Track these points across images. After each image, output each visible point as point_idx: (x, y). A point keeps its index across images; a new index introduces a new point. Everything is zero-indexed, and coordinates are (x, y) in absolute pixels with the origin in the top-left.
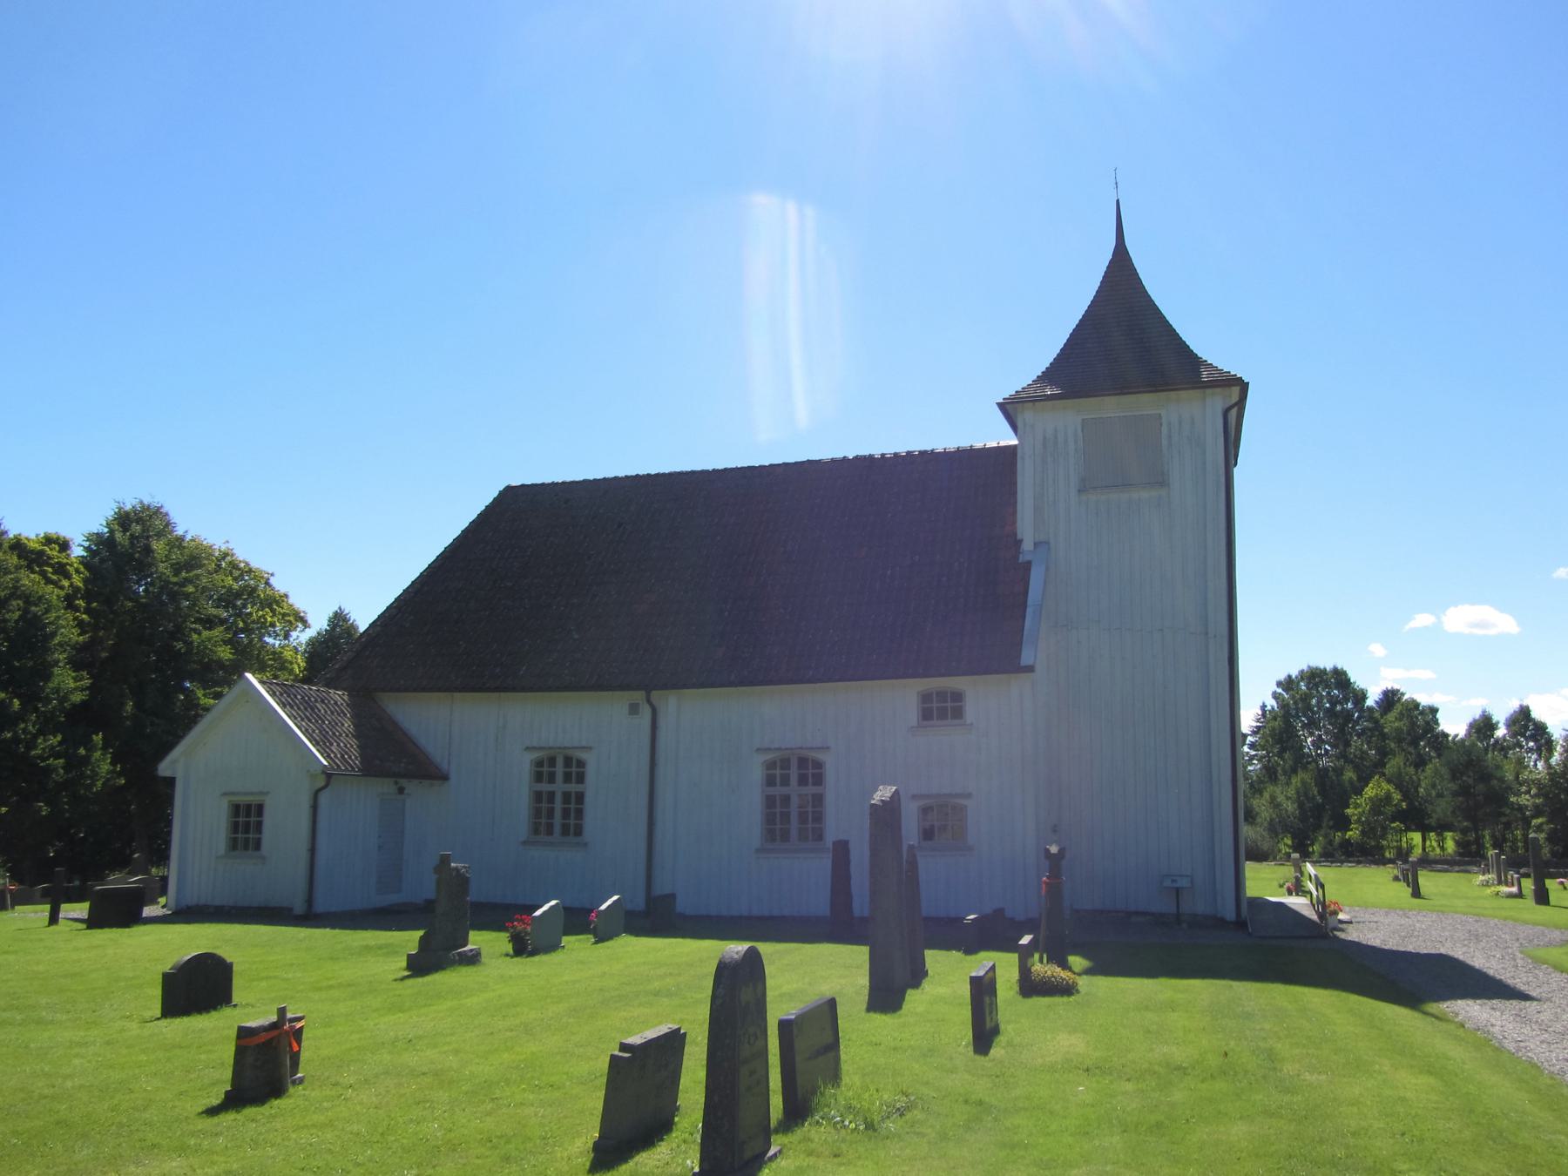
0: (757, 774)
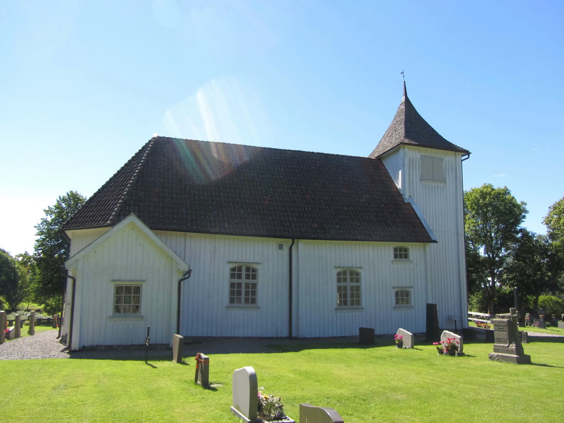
0: (335, 277)
